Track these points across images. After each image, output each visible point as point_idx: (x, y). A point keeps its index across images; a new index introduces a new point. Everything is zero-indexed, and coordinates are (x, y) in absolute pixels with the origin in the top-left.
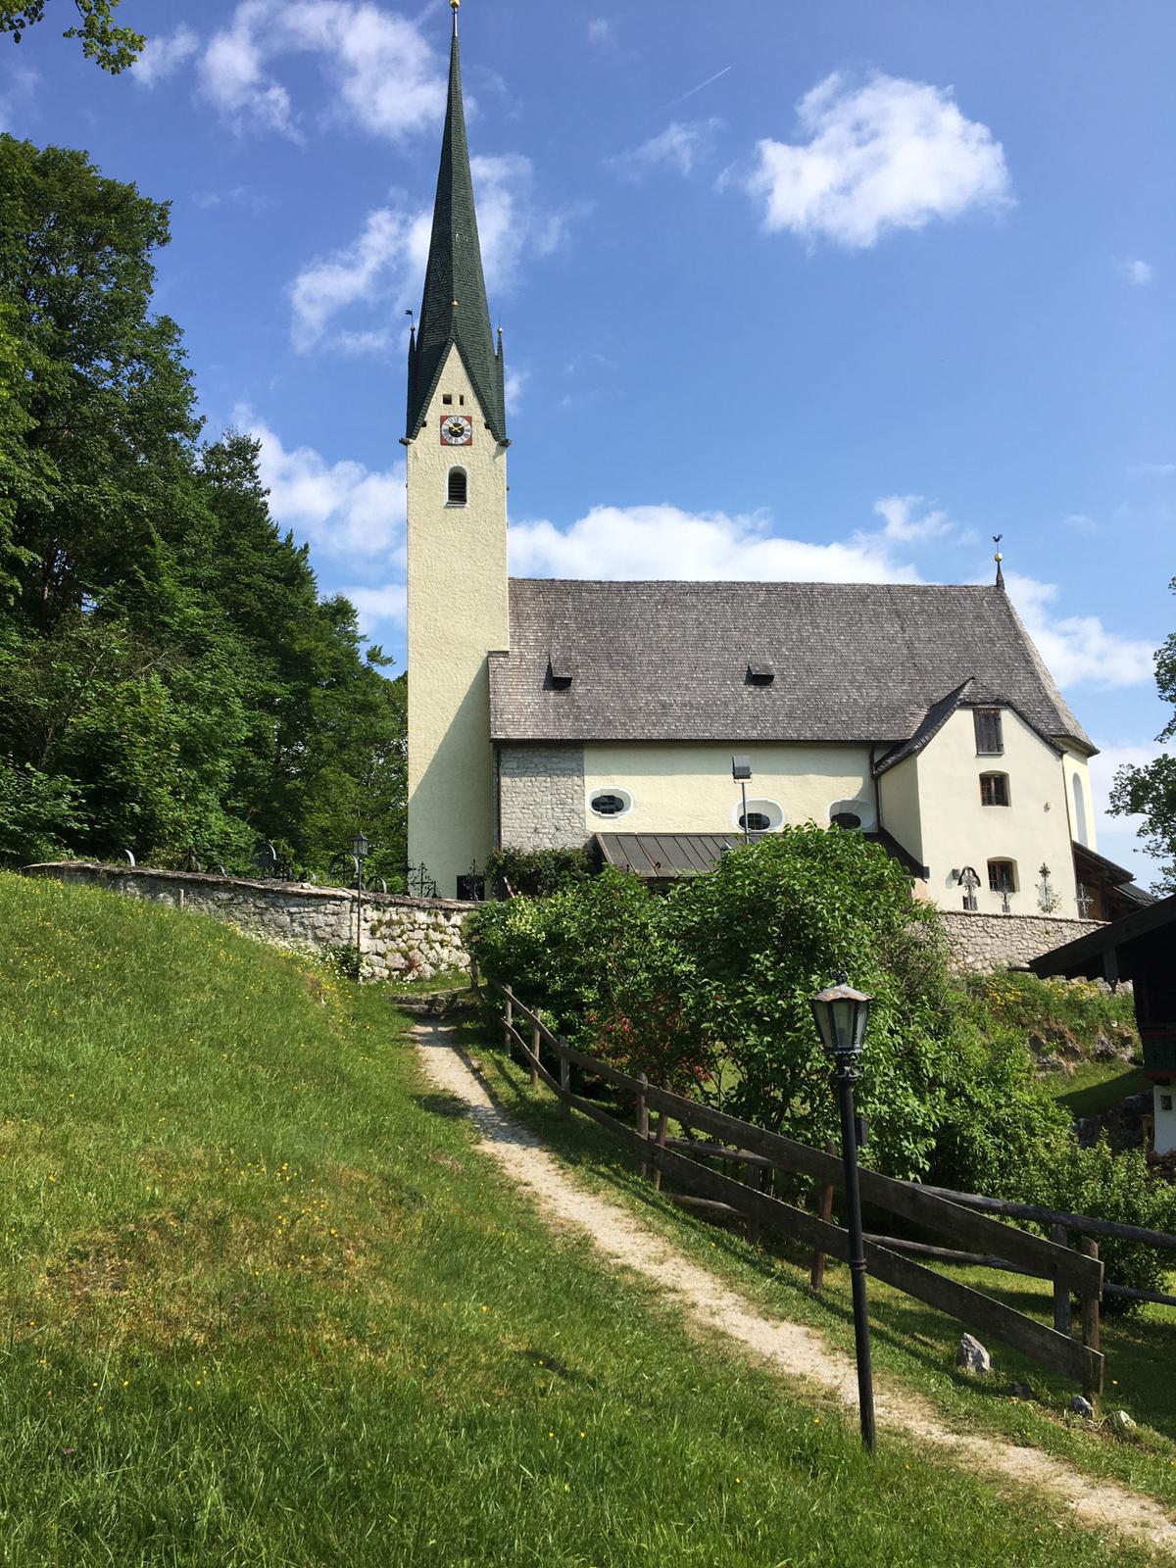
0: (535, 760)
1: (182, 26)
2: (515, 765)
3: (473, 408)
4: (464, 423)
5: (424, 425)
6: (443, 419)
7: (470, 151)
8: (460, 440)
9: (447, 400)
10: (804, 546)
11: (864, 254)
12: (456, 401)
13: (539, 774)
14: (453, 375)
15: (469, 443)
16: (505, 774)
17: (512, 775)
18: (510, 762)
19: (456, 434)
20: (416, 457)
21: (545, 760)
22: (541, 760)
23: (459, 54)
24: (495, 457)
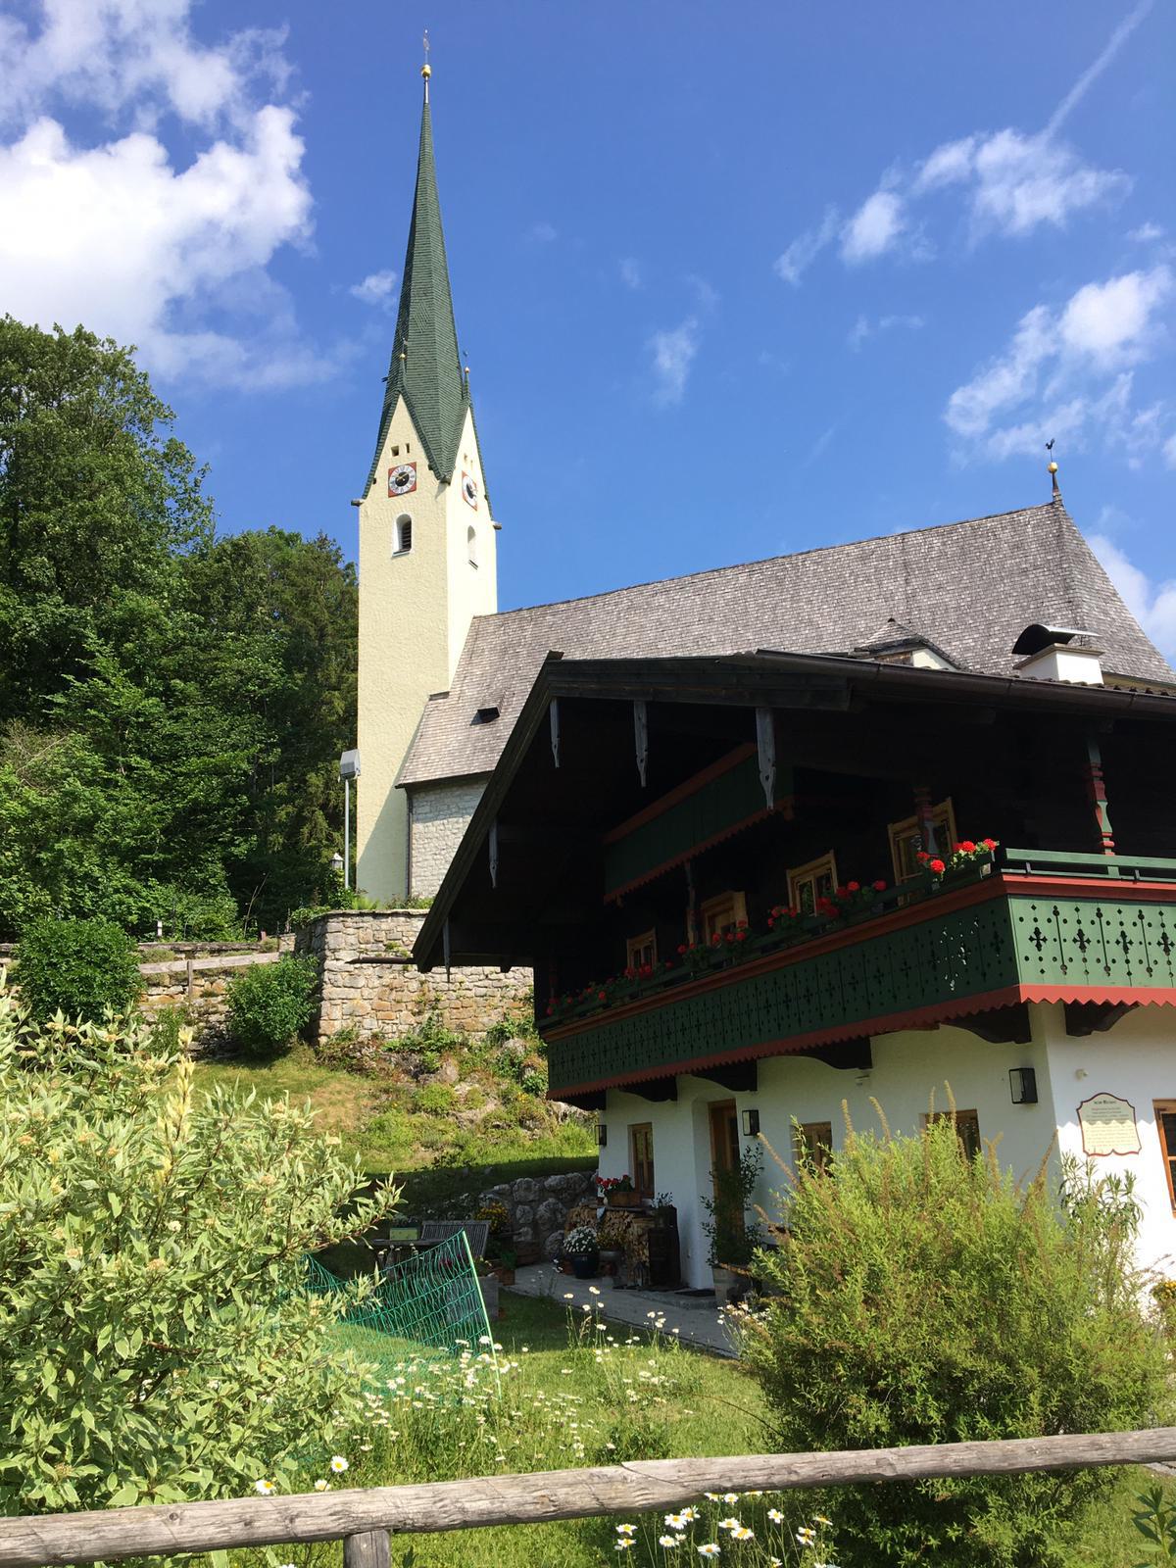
0: (447, 801)
1: (298, 118)
2: (427, 809)
3: (419, 455)
4: (408, 470)
5: (385, 379)
6: (391, 472)
7: (1057, 1121)
8: (405, 488)
9: (396, 452)
10: (1131, 569)
11: (306, 145)
12: (403, 451)
13: (451, 815)
14: (401, 410)
15: (414, 489)
16: (418, 820)
17: (425, 821)
18: (423, 806)
19: (401, 483)
20: (367, 516)
21: (458, 799)
22: (453, 800)
23: (436, 249)
24: (436, 497)
